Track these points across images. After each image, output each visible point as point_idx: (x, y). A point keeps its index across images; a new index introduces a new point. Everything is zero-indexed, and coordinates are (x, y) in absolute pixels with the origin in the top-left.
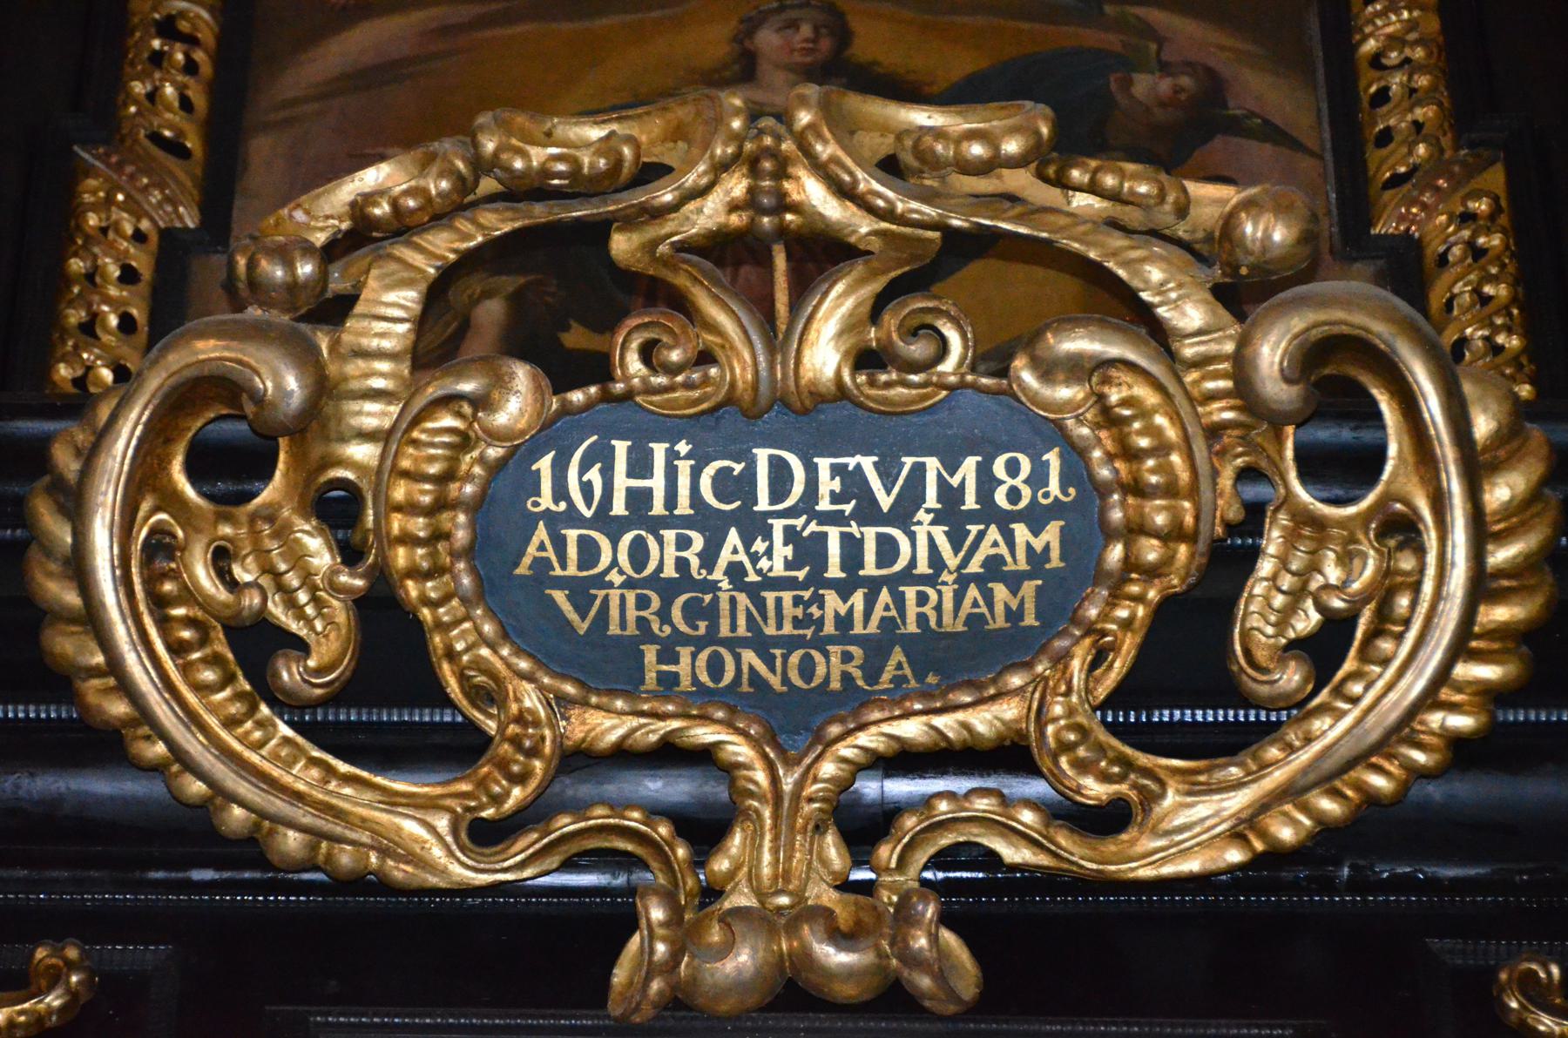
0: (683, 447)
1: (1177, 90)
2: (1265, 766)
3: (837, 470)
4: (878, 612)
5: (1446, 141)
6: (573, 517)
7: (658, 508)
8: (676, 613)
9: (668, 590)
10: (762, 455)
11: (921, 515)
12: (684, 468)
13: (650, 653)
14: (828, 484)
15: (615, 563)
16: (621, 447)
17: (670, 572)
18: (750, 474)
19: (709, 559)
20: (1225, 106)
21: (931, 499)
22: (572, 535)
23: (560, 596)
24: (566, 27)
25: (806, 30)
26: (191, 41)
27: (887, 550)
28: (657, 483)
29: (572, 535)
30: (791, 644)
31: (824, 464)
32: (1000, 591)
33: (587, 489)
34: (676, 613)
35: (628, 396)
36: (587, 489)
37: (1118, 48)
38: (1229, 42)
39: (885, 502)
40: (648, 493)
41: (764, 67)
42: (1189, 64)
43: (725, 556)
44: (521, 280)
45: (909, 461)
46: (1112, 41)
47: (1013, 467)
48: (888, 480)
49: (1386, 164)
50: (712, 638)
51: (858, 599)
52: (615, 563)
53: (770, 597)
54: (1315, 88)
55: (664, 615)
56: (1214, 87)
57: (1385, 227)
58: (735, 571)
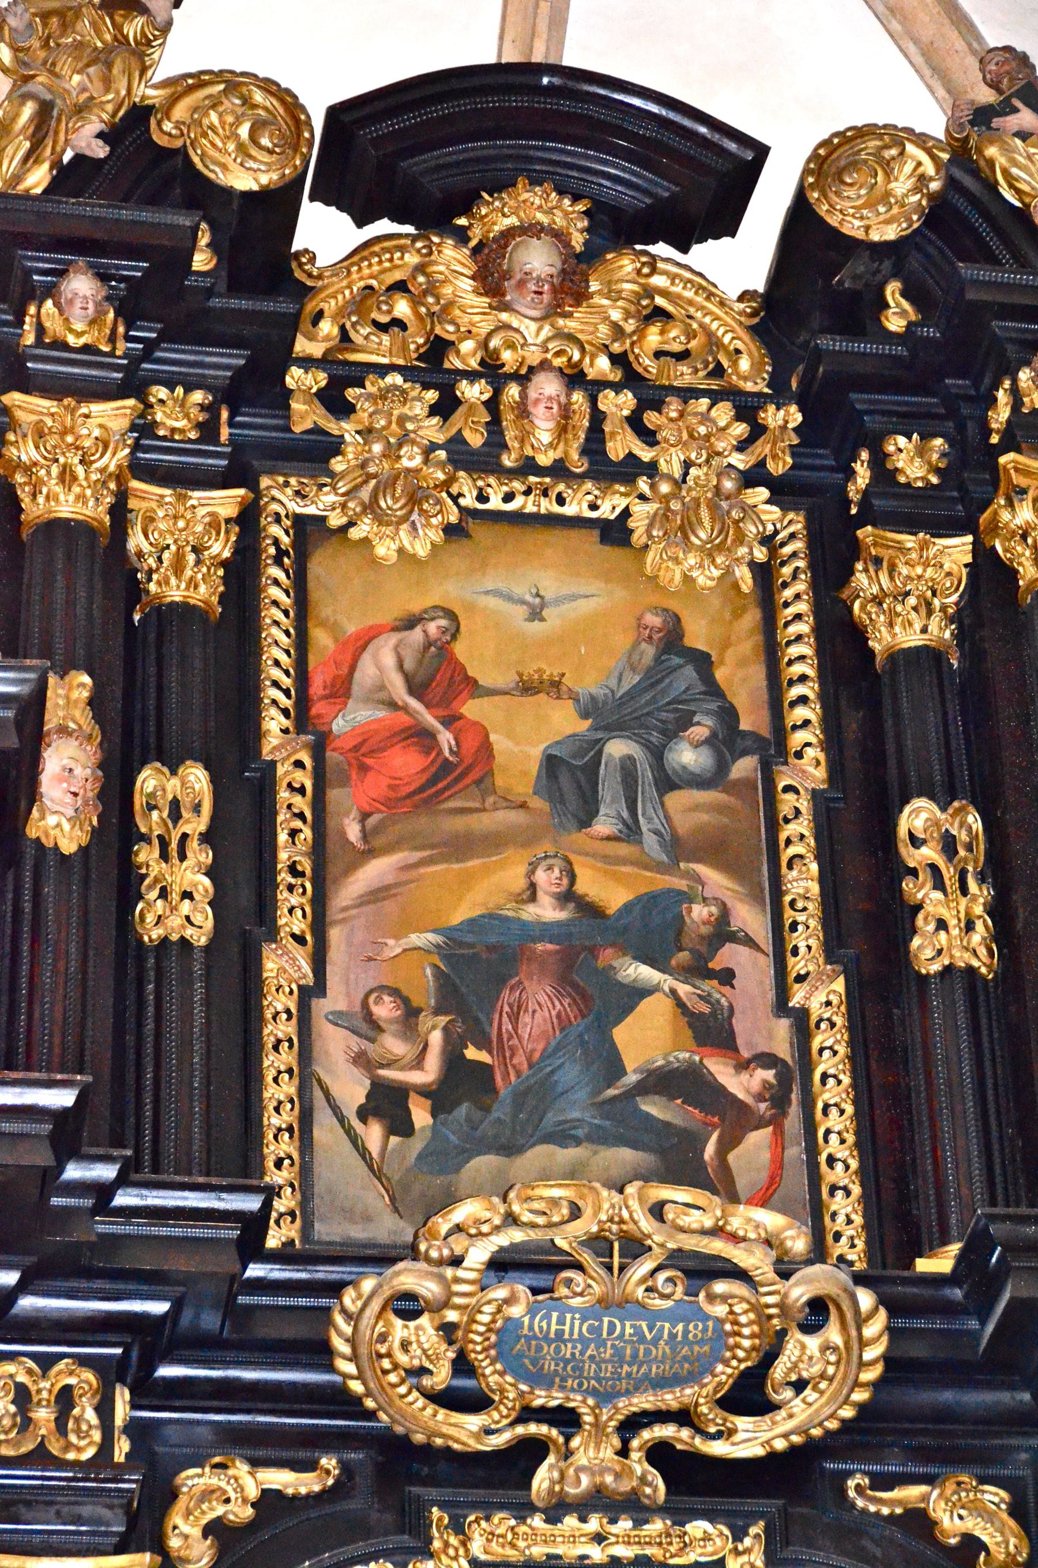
0: (577, 1316)
1: (711, 915)
2: (774, 1423)
3: (632, 1326)
4: (642, 1371)
5: (821, 960)
6: (535, 1337)
7: (566, 1336)
8: (569, 1368)
9: (567, 1362)
10: (606, 1320)
11: (662, 1342)
12: (577, 1323)
13: (557, 1380)
14: (629, 1330)
15: (548, 1352)
16: (555, 1315)
17: (568, 1356)
18: (600, 1327)
19: (582, 1353)
20: (728, 924)
21: (666, 1337)
22: (534, 1343)
23: (527, 1361)
24: (456, 866)
25: (557, 872)
26: (302, 874)
27: (648, 1352)
28: (567, 1328)
29: (534, 1343)
30: (607, 1379)
31: (628, 1324)
32: (686, 1365)
33: (541, 1328)
34: (569, 1368)
35: (560, 1299)
36: (541, 1328)
37: (686, 889)
38: (730, 885)
39: (649, 1337)
40: (563, 1331)
41: (540, 894)
42: (715, 899)
43: (589, 1352)
44: (448, 1018)
45: (659, 1324)
46: (681, 884)
47: (696, 1327)
48: (650, 1330)
49: (797, 965)
50: (579, 1377)
51: (635, 1368)
52: (548, 1352)
53: (603, 1366)
54: (764, 911)
55: (564, 1369)
56: (725, 914)
57: (795, 1002)
58: (592, 1358)
